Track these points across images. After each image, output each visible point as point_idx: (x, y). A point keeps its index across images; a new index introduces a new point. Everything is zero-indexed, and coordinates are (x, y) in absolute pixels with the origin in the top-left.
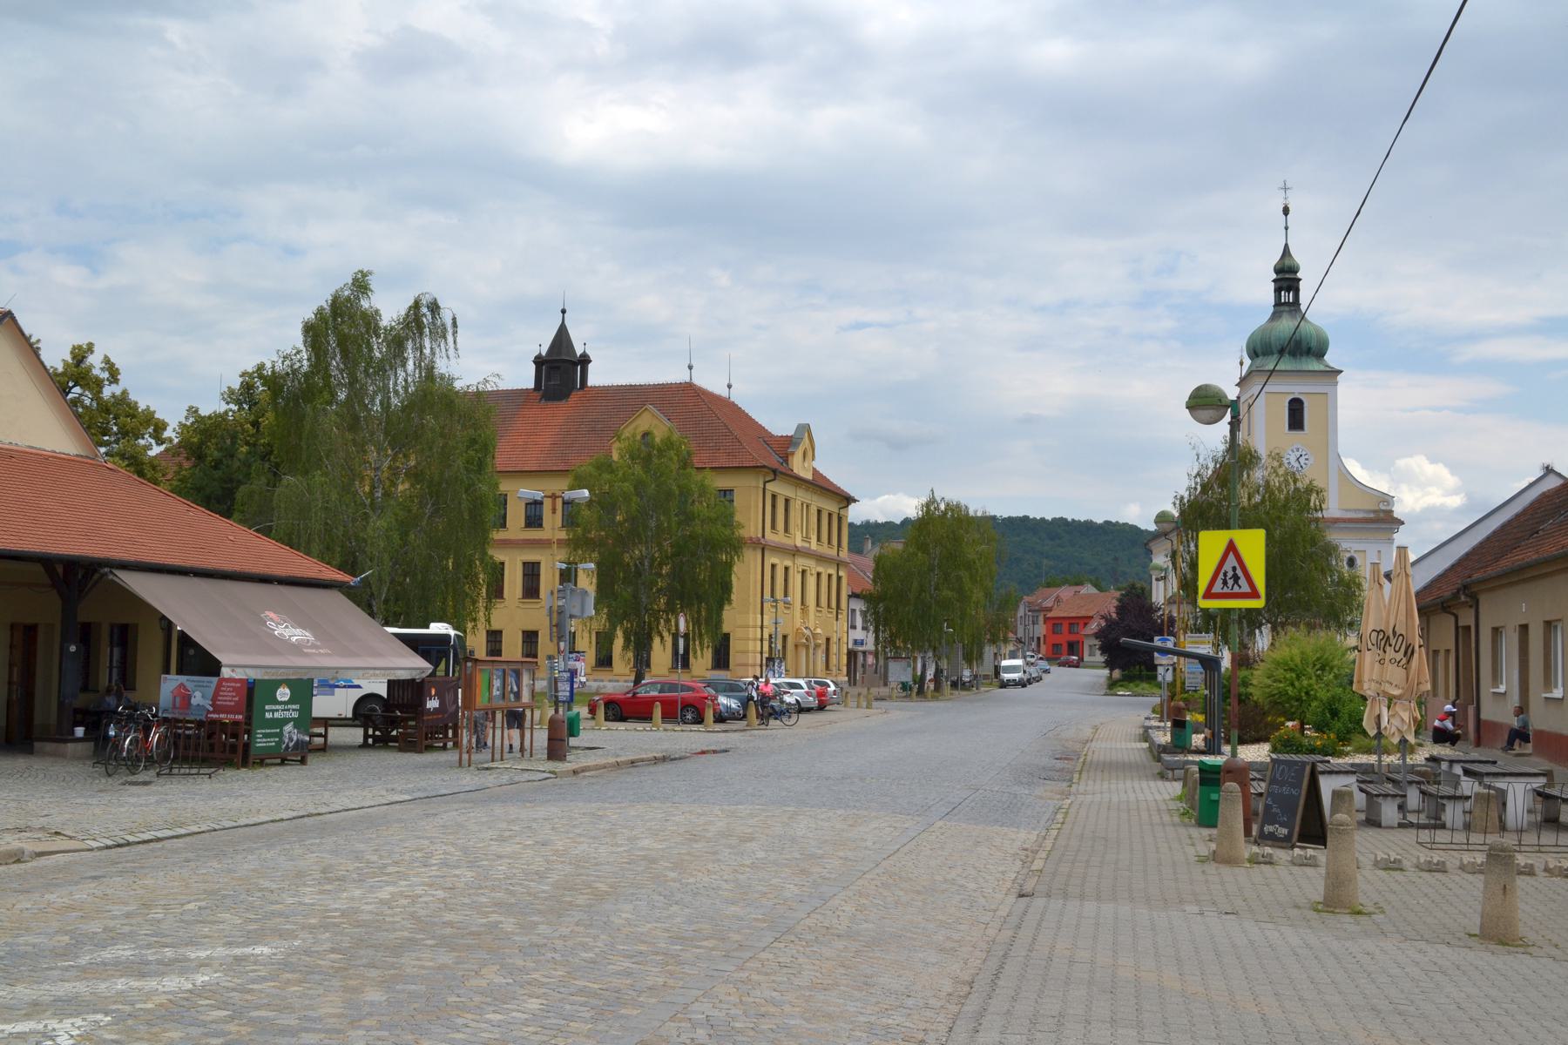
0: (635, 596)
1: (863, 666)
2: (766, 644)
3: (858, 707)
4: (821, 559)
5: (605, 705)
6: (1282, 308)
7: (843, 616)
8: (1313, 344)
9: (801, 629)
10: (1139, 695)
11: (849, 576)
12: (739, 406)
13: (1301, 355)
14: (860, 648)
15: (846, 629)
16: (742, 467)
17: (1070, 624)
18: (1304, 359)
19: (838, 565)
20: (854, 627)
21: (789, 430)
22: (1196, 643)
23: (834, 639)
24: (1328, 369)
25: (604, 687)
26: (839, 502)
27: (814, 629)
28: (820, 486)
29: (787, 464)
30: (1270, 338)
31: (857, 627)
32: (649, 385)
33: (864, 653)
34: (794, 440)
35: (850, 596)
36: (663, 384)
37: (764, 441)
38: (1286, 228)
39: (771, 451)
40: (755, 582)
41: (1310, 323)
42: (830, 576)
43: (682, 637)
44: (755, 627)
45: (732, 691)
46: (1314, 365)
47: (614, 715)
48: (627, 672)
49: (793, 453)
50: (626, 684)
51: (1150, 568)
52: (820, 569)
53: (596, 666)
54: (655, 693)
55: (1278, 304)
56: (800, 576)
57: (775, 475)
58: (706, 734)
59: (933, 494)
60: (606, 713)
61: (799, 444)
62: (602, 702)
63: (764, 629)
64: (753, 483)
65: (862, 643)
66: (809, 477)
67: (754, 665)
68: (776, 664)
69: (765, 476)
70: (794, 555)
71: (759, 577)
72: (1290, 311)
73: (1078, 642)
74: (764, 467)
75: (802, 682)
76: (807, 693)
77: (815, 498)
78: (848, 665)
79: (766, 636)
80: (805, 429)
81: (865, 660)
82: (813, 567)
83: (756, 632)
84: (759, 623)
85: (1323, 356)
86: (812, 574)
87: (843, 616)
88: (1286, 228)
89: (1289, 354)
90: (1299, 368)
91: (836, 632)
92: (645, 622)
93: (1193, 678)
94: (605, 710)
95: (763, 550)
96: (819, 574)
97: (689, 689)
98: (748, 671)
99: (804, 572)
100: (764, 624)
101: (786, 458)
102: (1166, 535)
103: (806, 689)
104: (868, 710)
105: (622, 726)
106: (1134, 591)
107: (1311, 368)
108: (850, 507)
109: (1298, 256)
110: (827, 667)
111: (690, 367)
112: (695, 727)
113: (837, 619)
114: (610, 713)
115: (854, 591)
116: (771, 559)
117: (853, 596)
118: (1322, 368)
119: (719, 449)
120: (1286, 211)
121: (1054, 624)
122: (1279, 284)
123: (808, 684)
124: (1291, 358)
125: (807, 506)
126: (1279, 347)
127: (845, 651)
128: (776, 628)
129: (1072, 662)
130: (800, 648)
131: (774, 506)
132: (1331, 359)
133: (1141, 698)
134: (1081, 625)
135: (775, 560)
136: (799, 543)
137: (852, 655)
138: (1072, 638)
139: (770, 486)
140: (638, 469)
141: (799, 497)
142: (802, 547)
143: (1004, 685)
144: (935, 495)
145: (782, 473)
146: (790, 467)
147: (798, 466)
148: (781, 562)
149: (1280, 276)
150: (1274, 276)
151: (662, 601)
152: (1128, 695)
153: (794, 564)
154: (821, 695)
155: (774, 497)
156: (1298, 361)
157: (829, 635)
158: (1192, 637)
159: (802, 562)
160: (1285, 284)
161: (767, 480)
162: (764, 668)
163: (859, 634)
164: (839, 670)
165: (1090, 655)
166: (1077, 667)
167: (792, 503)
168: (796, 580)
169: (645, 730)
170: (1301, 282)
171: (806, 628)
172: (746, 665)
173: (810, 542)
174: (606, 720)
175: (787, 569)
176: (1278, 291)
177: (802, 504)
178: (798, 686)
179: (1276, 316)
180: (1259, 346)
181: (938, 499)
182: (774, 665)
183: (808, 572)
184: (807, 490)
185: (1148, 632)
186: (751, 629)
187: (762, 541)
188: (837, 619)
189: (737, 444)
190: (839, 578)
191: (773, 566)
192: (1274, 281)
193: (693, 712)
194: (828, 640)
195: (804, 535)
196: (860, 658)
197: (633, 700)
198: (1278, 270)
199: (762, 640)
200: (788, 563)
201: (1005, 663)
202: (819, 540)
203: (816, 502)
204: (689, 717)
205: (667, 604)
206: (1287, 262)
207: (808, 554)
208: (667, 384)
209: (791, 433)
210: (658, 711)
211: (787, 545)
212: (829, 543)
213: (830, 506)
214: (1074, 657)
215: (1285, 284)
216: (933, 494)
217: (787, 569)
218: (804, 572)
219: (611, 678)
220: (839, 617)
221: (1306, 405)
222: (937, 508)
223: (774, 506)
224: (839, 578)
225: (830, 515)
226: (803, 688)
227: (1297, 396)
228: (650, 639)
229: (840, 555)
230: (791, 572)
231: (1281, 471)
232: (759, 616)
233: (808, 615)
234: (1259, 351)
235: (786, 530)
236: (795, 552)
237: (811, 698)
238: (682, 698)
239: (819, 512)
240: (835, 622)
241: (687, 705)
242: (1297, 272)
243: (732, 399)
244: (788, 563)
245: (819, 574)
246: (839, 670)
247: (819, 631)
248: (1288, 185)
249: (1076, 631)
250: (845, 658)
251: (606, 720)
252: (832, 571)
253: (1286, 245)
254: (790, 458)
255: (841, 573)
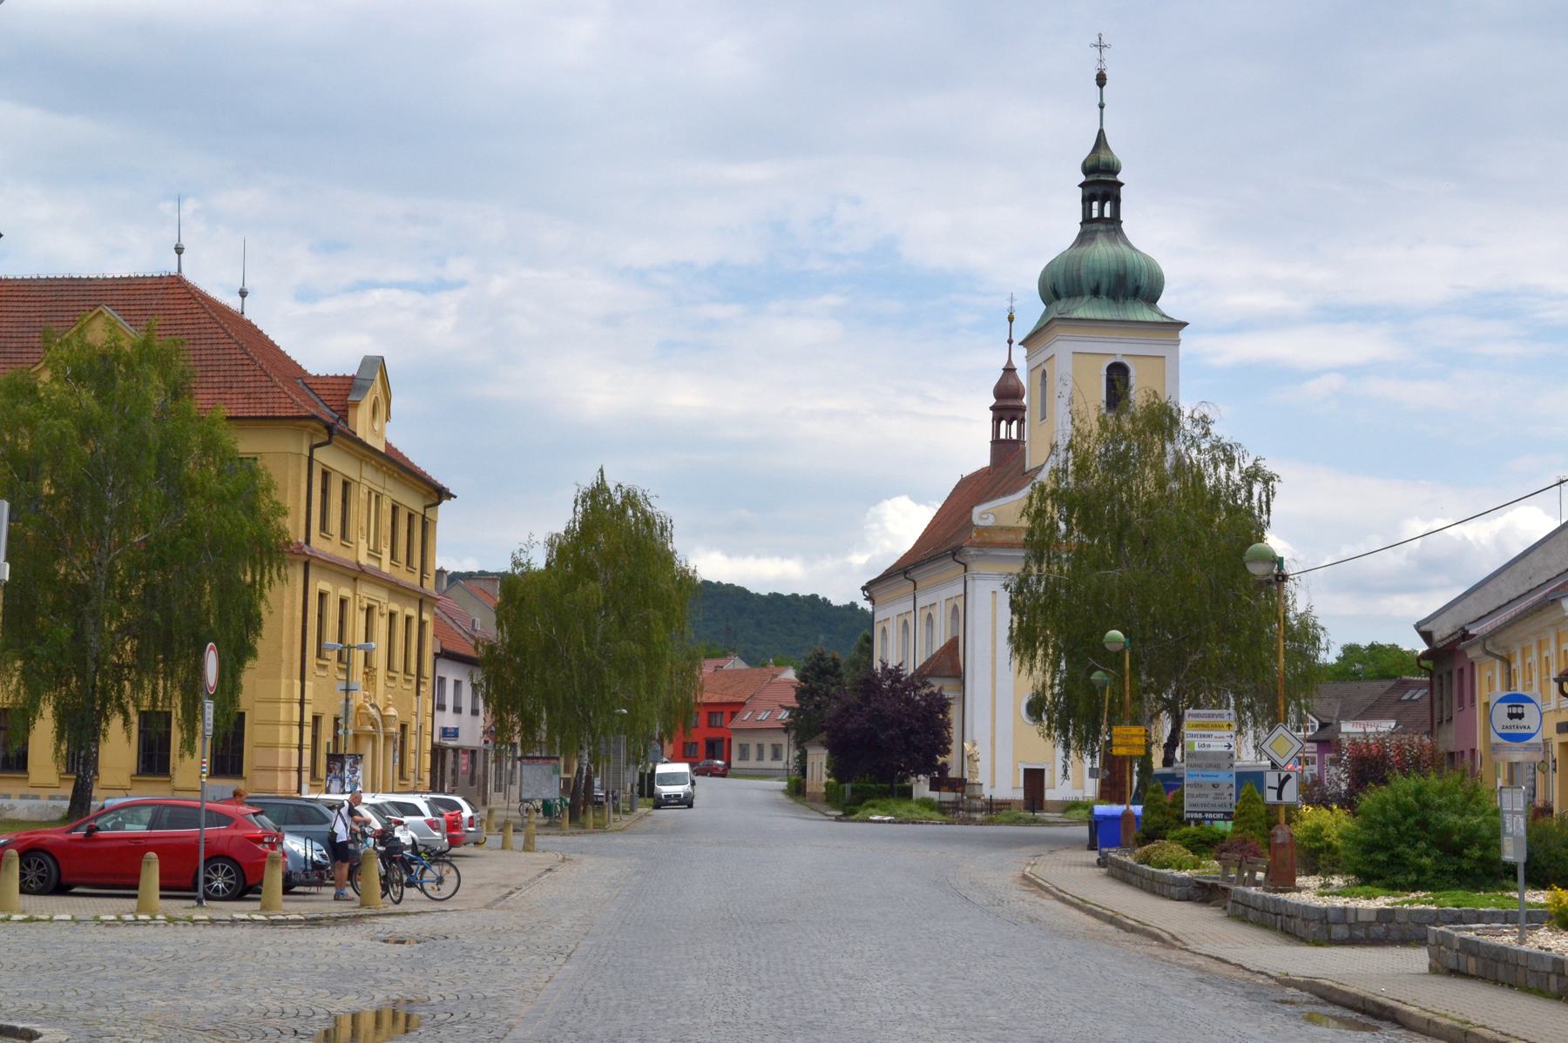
0: (77, 637)
1: (454, 772)
2: (308, 731)
3: (503, 848)
4: (396, 589)
5: (20, 856)
6: (1095, 226)
7: (426, 689)
8: (1144, 281)
9: (366, 708)
10: (907, 822)
11: (438, 621)
12: (259, 328)
13: (1126, 298)
14: (451, 743)
15: (430, 711)
16: (273, 418)
17: (710, 713)
18: (1129, 303)
19: (421, 602)
20: (442, 708)
21: (348, 366)
22: (1205, 726)
23: (413, 727)
24: (1165, 320)
25: (12, 808)
26: (425, 497)
27: (385, 709)
28: (394, 465)
29: (346, 423)
30: (1079, 270)
31: (463, 710)
32: (105, 279)
33: (456, 750)
34: (358, 382)
35: (437, 656)
36: (129, 278)
37: (305, 384)
38: (1102, 106)
39: (317, 400)
40: (292, 621)
41: (1137, 250)
42: (408, 619)
43: (211, 697)
44: (290, 701)
45: (303, 822)
46: (1144, 314)
47: (41, 879)
48: (54, 779)
49: (356, 404)
50: (52, 803)
51: (1245, 558)
52: (395, 607)
53: (138, 774)
54: (136, 829)
55: (1087, 220)
56: (363, 616)
57: (330, 434)
58: (269, 929)
59: (602, 475)
60: (22, 876)
61: (367, 389)
62: (14, 852)
63: (306, 706)
64: (293, 449)
65: (455, 733)
66: (382, 448)
67: (287, 770)
68: (347, 767)
69: (312, 435)
70: (355, 579)
71: (299, 614)
72: (1108, 231)
73: (723, 740)
74: (313, 418)
75: (420, 801)
76: (430, 823)
77: (389, 484)
78: (433, 771)
79: (308, 718)
80: (375, 366)
81: (456, 763)
82: (380, 597)
83: (291, 709)
84: (297, 695)
85: (1155, 303)
86: (382, 615)
87: (426, 689)
88: (1102, 106)
89: (1108, 295)
90: (1122, 316)
91: (416, 716)
92: (94, 686)
93: (1199, 796)
94: (21, 868)
95: (306, 566)
96: (392, 615)
97: (218, 818)
98: (277, 777)
99: (369, 610)
100: (306, 697)
101: (344, 411)
102: (906, 573)
103: (429, 816)
104: (529, 855)
105: (60, 908)
106: (822, 664)
107: (1140, 318)
108: (440, 506)
109: (1118, 148)
110: (402, 775)
111: (179, 250)
112: (240, 910)
113: (418, 693)
114: (32, 875)
115: (445, 646)
116: (319, 584)
117: (444, 655)
118: (1157, 318)
119: (231, 388)
120: (1101, 80)
121: (710, 713)
122: (1090, 190)
123: (433, 804)
124: (1111, 301)
125: (377, 497)
126: (1093, 285)
127: (429, 747)
128: (347, 700)
129: (716, 769)
130: (362, 741)
131: (325, 491)
132: (1169, 304)
133: (910, 826)
134: (727, 715)
135: (324, 585)
136: (364, 560)
137: (438, 752)
138: (714, 734)
139: (322, 455)
140: (87, 397)
141: (367, 479)
142: (368, 566)
143: (661, 803)
144: (605, 478)
145: (342, 433)
146: (351, 427)
147: (362, 424)
148: (337, 590)
149: (1092, 178)
150: (1082, 178)
151: (128, 647)
152: (889, 822)
153: (355, 594)
154: (453, 825)
155: (325, 475)
156: (1120, 306)
157: (406, 719)
158: (1197, 716)
159: (367, 593)
160: (1099, 190)
161: (315, 442)
162: (306, 775)
163: (447, 719)
164: (419, 779)
165: (740, 759)
166: (723, 775)
167: (353, 488)
168: (381, 625)
169: (119, 919)
170: (1122, 188)
171: (373, 706)
172: (274, 769)
173: (380, 559)
174: (22, 891)
175: (343, 602)
176: (1087, 200)
177: (369, 493)
178: (416, 811)
179: (1084, 238)
180: (1061, 282)
181: (611, 486)
182: (342, 769)
183: (376, 611)
184: (377, 470)
185: (906, 720)
186: (282, 705)
187: (306, 549)
188: (418, 693)
189: (264, 379)
190: (422, 624)
191: (322, 596)
192: (1082, 185)
193: (228, 872)
194: (403, 727)
195: (372, 548)
196: (450, 755)
197: (85, 845)
198: (1088, 169)
199: (301, 725)
200: (346, 592)
201: (661, 769)
202: (393, 557)
203: (393, 492)
204: (219, 883)
205: (137, 653)
206: (1103, 157)
207: (377, 579)
208: (137, 277)
209: (351, 369)
210: (151, 874)
211: (346, 561)
212: (408, 563)
213: (412, 502)
214: (719, 762)
215: (1099, 190)
216: (602, 475)
217: (343, 602)
218: (369, 610)
219: (24, 791)
220: (422, 689)
221: (1132, 373)
222: (610, 500)
223: (325, 491)
224: (422, 624)
225: (410, 516)
226: (420, 814)
227: (1119, 359)
228: (103, 715)
229: (425, 585)
230: (350, 606)
231: (1205, 445)
232: (297, 683)
233: (374, 684)
234: (1062, 290)
235: (344, 535)
236: (357, 574)
237: (437, 834)
238: (207, 842)
239: (395, 509)
240: (415, 698)
241: (217, 857)
242: (1116, 173)
243: (247, 316)
244: (346, 592)
245: (392, 615)
246: (419, 779)
247: (392, 711)
248: (1105, 41)
249: (718, 724)
250: (428, 757)
251: (22, 891)
252: (412, 611)
253: (1101, 132)
254: (351, 413)
255: (426, 616)
